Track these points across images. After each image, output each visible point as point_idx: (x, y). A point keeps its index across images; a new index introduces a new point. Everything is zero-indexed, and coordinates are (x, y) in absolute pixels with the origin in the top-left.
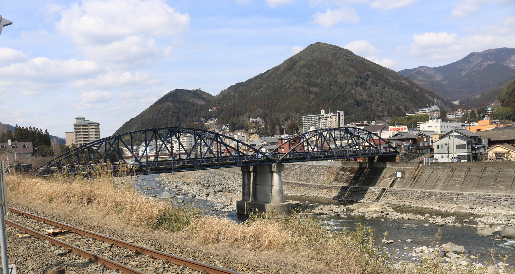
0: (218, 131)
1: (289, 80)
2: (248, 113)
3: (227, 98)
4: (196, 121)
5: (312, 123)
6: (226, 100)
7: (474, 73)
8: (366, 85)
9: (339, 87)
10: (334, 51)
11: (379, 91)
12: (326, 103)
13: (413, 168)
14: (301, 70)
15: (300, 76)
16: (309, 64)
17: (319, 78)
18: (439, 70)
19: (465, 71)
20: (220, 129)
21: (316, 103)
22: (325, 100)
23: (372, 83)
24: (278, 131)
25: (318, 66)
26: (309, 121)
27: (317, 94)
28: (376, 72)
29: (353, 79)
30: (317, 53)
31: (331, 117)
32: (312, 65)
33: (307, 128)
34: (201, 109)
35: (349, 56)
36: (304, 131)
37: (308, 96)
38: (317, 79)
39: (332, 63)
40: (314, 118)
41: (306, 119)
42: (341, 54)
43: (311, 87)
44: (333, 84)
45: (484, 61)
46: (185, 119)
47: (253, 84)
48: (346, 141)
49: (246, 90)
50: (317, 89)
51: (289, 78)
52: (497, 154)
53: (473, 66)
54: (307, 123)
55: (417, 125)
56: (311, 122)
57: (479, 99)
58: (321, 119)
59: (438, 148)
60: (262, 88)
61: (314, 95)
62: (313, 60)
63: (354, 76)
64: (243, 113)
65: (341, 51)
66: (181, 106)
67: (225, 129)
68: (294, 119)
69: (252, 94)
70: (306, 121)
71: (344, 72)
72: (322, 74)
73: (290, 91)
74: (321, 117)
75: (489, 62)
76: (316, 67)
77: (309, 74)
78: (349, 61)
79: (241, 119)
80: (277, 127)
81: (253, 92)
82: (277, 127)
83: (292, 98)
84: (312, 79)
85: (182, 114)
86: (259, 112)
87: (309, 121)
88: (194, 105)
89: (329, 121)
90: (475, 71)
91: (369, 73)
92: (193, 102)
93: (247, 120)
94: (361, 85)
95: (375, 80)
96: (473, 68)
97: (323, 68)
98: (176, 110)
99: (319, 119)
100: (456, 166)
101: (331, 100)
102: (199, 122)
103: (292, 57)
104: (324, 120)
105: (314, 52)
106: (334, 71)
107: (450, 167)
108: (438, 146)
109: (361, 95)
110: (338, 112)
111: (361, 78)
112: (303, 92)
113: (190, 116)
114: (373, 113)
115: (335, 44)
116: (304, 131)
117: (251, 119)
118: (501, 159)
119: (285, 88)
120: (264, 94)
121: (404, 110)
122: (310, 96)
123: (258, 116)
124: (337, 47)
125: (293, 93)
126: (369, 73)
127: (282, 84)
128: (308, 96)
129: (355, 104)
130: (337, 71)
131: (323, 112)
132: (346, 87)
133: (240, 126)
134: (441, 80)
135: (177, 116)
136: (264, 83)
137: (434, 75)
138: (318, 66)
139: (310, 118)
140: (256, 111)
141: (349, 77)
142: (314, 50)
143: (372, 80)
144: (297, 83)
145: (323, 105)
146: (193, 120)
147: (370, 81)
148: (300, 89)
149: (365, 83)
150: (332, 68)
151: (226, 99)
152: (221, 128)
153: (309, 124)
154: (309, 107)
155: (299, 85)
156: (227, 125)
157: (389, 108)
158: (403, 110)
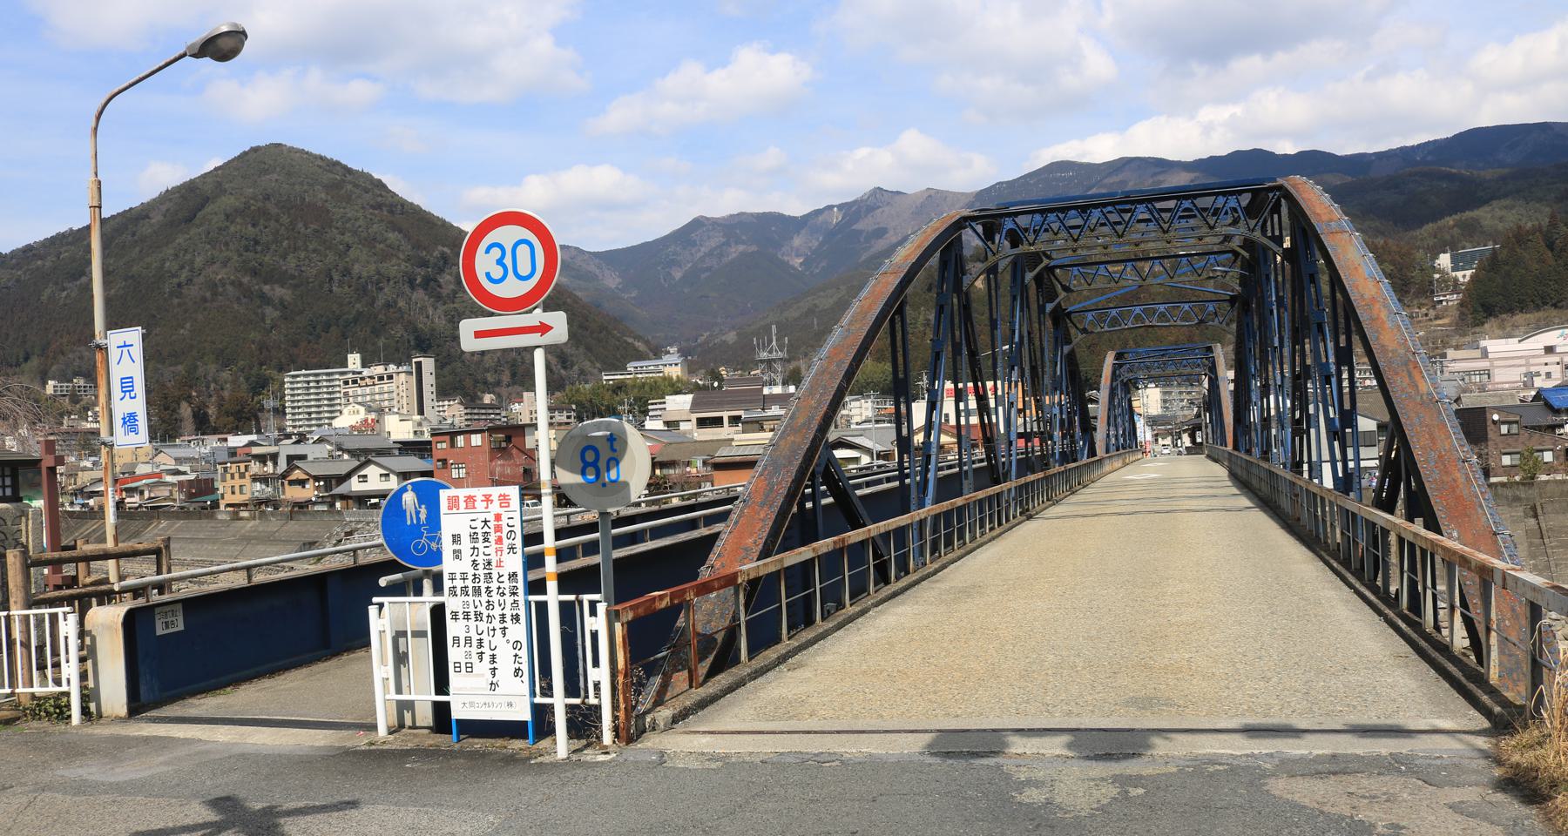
1: (188, 257)
2: (34, 362)
5: (320, 396)
7: (707, 274)
8: (440, 286)
10: (332, 176)
12: (319, 337)
14: (227, 227)
15: (227, 244)
16: (253, 208)
18: (610, 258)
19: (680, 266)
24: (188, 424)
25: (286, 217)
26: (308, 388)
29: (399, 265)
31: (390, 377)
32: (264, 213)
38: (284, 257)
40: (326, 381)
41: (298, 382)
43: (266, 284)
44: (336, 277)
45: (727, 244)
47: (48, 264)
49: (18, 281)
50: (284, 291)
51: (186, 251)
53: (701, 254)
54: (300, 398)
55: (650, 407)
57: (735, 343)
58: (355, 382)
61: (276, 310)
62: (265, 199)
63: (402, 256)
69: (44, 298)
71: (370, 242)
72: (300, 243)
73: (193, 292)
74: (350, 376)
75: (741, 248)
76: (277, 221)
77: (257, 242)
78: (381, 209)
80: (186, 411)
82: (186, 411)
83: (200, 317)
84: (267, 259)
87: (308, 388)
89: (386, 389)
90: (709, 269)
91: (446, 249)
93: (37, 387)
96: (702, 259)
99: (346, 383)
100: (1541, 494)
103: (192, 182)
104: (367, 386)
105: (266, 172)
106: (339, 238)
107: (1517, 499)
110: (414, 360)
111: (424, 264)
112: (238, 299)
114: (470, 375)
115: (331, 154)
117: (51, 383)
119: (175, 280)
121: (559, 367)
122: (264, 315)
123: (77, 374)
124: (338, 163)
125: (205, 300)
127: (162, 267)
129: (412, 343)
130: (348, 238)
131: (354, 360)
132: (381, 289)
134: (617, 288)
137: (597, 271)
138: (286, 217)
139: (311, 378)
141: (385, 257)
145: (310, 342)
147: (451, 274)
148: (230, 288)
149: (436, 281)
150: (330, 227)
154: (263, 347)
157: (515, 360)
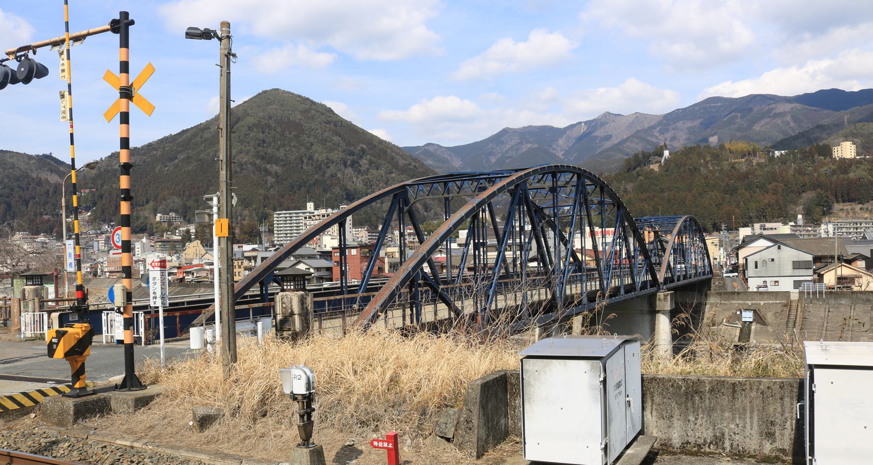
0: (94, 234)
2: (151, 204)
3: (110, 174)
4: (46, 214)
5: (292, 225)
6: (108, 178)
8: (360, 166)
9: (316, 167)
11: (382, 177)
13: (776, 303)
15: (248, 143)
16: (262, 123)
17: (282, 149)
20: (99, 232)
21: (278, 192)
22: (293, 188)
23: (371, 163)
26: (286, 221)
27: (278, 177)
28: (375, 146)
29: (338, 154)
30: (275, 106)
33: (281, 234)
34: (55, 192)
35: (330, 117)
36: (276, 239)
37: (263, 180)
39: (302, 125)
40: (296, 217)
41: (281, 217)
42: (317, 111)
44: (305, 160)
46: (23, 208)
47: (159, 153)
48: (511, 253)
49: (144, 162)
50: (277, 168)
52: (840, 279)
54: (281, 225)
56: (291, 224)
58: (310, 218)
59: (756, 267)
60: (176, 161)
61: (273, 177)
63: (340, 149)
64: (141, 204)
65: (314, 107)
66: (14, 184)
67: (107, 231)
68: (239, 218)
69: (157, 171)
70: (281, 221)
71: (324, 142)
72: (286, 142)
74: (308, 214)
75: (529, 146)
76: (275, 130)
77: (264, 142)
78: (330, 125)
79: (141, 213)
81: (159, 167)
85: (17, 199)
86: (174, 202)
87: (286, 221)
88: (39, 183)
90: (510, 157)
91: (364, 146)
92: (37, 177)
93: (152, 216)
94: (352, 165)
95: (376, 159)
96: (507, 152)
97: (287, 133)
98: (3, 190)
101: (303, 189)
102: (53, 216)
104: (316, 220)
105: (270, 104)
106: (307, 139)
108: (756, 263)
109: (353, 183)
111: (352, 154)
112: (254, 172)
113: (34, 203)
116: (276, 239)
118: (849, 287)
120: (180, 170)
123: (171, 211)
124: (308, 99)
126: (364, 146)
128: (263, 180)
129: (344, 196)
130: (312, 139)
131: (310, 206)
132: (329, 167)
133: (138, 227)
134: (460, 167)
135: (6, 202)
136: (180, 152)
137: (449, 158)
139: (288, 215)
140: (169, 201)
141: (331, 150)
142: (270, 101)
143: (370, 159)
144: (242, 154)
145: (290, 195)
146: (40, 211)
147: (366, 159)
148: (249, 166)
149: (358, 163)
150: (303, 134)
151: (107, 176)
152: (100, 229)
153: (285, 227)
155: (245, 159)
156: (112, 223)
158: (421, 211)
